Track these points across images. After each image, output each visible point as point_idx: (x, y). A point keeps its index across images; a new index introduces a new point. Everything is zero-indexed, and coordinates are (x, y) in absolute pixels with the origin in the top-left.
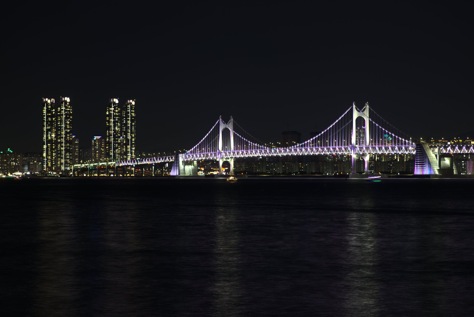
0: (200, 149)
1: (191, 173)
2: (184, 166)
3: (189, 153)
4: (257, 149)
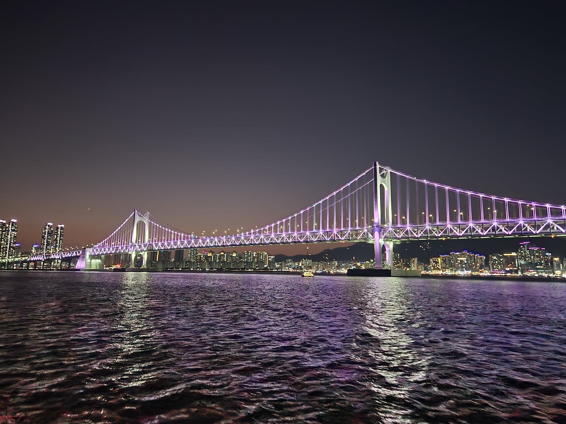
0: (110, 244)
1: (98, 267)
2: (91, 260)
3: (97, 247)
4: (184, 239)
